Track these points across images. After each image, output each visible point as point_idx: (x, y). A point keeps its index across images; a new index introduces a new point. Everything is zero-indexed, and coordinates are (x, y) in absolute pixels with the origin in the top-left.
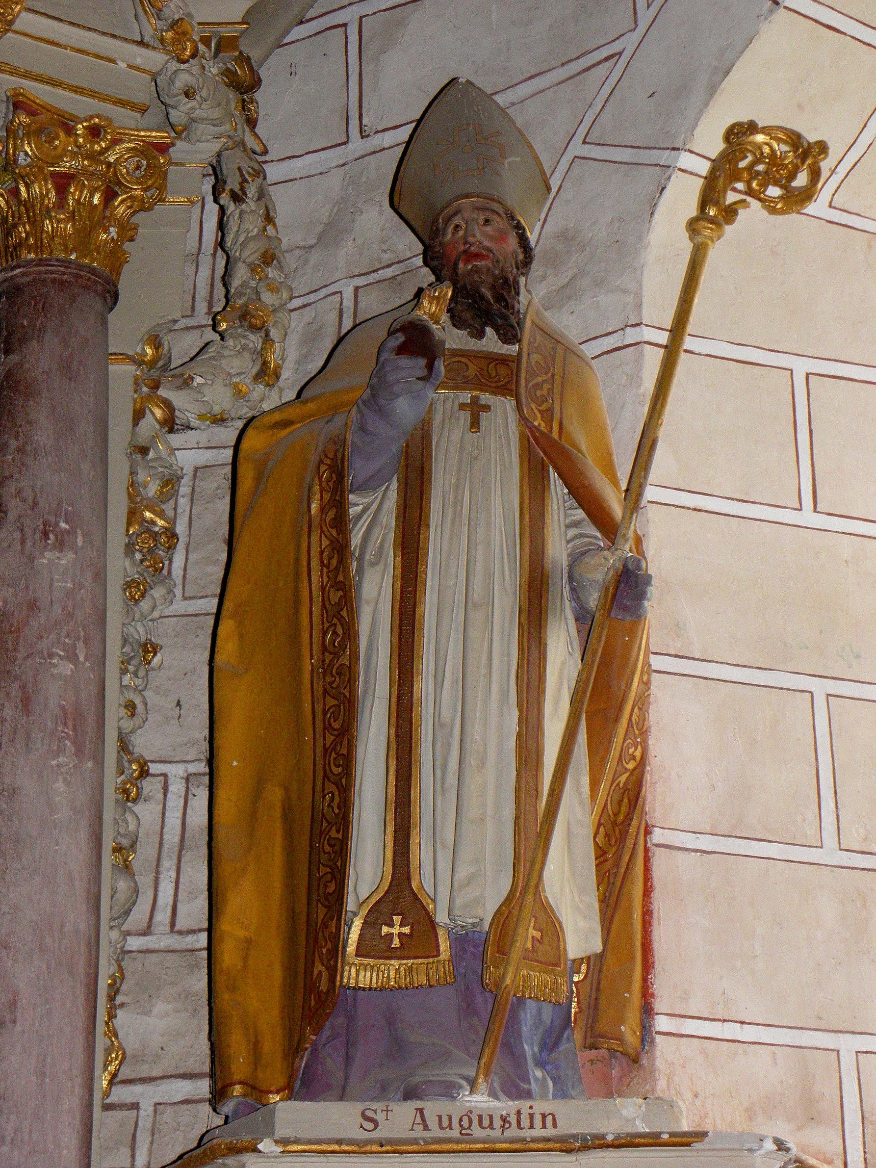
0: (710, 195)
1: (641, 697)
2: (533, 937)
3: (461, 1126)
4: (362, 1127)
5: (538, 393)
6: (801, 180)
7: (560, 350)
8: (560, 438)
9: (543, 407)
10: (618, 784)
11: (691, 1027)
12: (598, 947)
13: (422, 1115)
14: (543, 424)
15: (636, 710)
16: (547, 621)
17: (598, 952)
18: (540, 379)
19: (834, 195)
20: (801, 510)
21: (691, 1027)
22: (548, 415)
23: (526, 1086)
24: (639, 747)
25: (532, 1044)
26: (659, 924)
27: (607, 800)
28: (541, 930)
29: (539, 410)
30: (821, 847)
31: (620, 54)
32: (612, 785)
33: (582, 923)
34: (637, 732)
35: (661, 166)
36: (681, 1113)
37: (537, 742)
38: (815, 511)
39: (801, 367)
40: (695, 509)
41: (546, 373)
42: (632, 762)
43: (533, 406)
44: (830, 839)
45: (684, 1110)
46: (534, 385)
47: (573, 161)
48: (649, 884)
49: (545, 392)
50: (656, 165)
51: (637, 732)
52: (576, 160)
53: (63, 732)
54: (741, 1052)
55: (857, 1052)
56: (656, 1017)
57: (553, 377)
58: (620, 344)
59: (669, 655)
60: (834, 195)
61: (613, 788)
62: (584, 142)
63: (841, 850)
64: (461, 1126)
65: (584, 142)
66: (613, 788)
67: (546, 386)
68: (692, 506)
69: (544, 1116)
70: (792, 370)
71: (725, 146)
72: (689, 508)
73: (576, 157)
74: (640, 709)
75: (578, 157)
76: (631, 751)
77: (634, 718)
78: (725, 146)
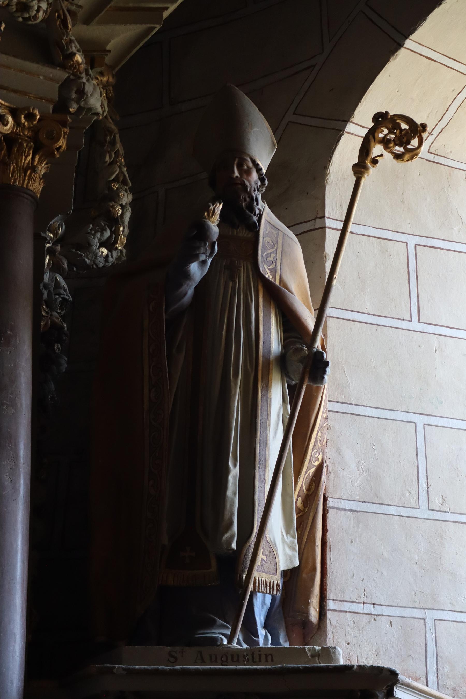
0: (365, 150)
1: (322, 426)
2: (262, 559)
3: (222, 660)
4: (169, 660)
6: (414, 143)
7: (280, 234)
8: (280, 284)
9: (271, 267)
10: (309, 474)
11: (346, 606)
12: (297, 563)
13: (201, 655)
14: (271, 277)
15: (319, 433)
17: (297, 566)
18: (270, 252)
19: (430, 146)
20: (411, 321)
21: (346, 606)
22: (274, 272)
23: (256, 639)
24: (321, 453)
25: (260, 616)
26: (330, 551)
27: (303, 482)
28: (265, 555)
29: (269, 269)
30: (419, 508)
31: (314, 66)
32: (305, 474)
33: (289, 552)
34: (320, 445)
35: (336, 130)
36: (339, 654)
37: (266, 453)
38: (419, 322)
39: (413, 241)
40: (353, 321)
41: (273, 248)
42: (317, 461)
43: (265, 266)
44: (423, 503)
45: (341, 653)
47: (288, 124)
48: (325, 529)
50: (334, 129)
51: (320, 445)
53: (9, 446)
54: (373, 620)
55: (435, 620)
56: (328, 601)
58: (312, 228)
59: (338, 402)
60: (430, 146)
61: (306, 476)
62: (294, 114)
63: (429, 510)
64: (222, 660)
65: (294, 114)
66: (306, 476)
67: (273, 255)
69: (266, 656)
70: (407, 243)
71: (373, 124)
72: (350, 320)
74: (321, 432)
76: (316, 455)
77: (318, 437)
78: (373, 124)
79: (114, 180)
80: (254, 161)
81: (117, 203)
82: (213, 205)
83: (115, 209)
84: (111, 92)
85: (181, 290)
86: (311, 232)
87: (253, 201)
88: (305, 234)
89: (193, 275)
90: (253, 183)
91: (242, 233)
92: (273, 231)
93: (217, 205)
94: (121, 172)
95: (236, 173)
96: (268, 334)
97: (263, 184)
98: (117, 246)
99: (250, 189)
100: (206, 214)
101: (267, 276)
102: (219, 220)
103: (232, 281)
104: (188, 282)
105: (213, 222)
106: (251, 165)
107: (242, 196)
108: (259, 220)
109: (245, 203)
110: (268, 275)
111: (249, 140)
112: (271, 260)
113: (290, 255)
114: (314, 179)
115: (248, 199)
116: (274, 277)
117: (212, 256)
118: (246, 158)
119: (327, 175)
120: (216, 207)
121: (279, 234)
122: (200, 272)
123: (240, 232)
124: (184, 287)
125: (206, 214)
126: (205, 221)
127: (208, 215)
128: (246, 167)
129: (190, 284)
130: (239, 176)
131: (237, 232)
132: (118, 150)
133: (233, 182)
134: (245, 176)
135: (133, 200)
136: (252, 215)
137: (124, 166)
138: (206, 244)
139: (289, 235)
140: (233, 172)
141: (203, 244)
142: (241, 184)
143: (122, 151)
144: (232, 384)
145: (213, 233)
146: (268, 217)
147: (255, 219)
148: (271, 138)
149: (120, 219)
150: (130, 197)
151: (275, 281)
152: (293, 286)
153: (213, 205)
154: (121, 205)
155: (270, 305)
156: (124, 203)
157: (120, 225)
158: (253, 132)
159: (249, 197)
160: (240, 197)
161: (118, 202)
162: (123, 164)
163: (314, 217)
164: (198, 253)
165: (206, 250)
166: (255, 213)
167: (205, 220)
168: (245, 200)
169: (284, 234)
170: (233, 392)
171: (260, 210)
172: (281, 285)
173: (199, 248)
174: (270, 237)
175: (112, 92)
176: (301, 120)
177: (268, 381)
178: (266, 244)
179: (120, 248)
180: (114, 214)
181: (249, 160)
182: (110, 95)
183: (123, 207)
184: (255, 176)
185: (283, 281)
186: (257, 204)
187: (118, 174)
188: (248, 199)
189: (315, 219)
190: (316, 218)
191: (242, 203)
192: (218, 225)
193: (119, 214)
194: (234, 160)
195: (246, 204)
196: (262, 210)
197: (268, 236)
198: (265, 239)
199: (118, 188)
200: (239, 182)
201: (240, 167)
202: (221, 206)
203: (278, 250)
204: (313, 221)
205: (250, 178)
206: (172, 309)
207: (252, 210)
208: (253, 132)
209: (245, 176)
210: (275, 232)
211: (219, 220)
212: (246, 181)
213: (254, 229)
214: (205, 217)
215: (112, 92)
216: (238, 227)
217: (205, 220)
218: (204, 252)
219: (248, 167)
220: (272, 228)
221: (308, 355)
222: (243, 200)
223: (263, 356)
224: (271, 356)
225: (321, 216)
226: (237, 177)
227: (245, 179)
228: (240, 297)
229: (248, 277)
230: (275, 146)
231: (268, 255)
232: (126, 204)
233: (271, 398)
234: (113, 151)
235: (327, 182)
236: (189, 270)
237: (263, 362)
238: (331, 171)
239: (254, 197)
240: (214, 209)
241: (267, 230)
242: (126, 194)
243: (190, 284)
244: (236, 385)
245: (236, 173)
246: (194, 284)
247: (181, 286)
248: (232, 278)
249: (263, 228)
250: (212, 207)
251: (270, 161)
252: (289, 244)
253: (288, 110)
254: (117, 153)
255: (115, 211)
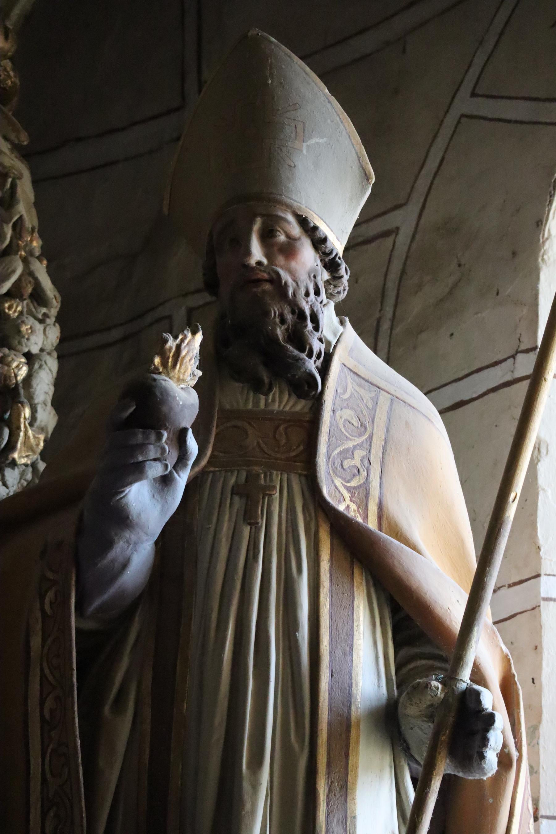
5: (346, 464)
7: (384, 399)
8: (380, 529)
9: (354, 483)
14: (353, 507)
16: (356, 776)
18: (350, 444)
22: (362, 495)
29: (348, 489)
41: (360, 435)
43: (338, 482)
46: (340, 453)
47: (459, 122)
49: (357, 461)
52: (464, 120)
57: (371, 438)
62: (474, 95)
65: (474, 95)
67: (359, 454)
68: (518, 616)
73: (463, 116)
75: (467, 116)
79: (9, 295)
80: (303, 222)
81: (15, 349)
82: (176, 338)
83: (9, 365)
84: (9, 76)
85: (111, 555)
86: (506, 390)
87: (301, 323)
88: (492, 395)
89: (139, 515)
90: (303, 277)
91: (280, 402)
92: (362, 392)
93: (185, 337)
94: (29, 273)
95: (257, 253)
96: (344, 652)
97: (335, 277)
98: (16, 455)
99: (294, 294)
100: (157, 360)
101: (341, 508)
102: (199, 373)
103: (250, 524)
104: (127, 534)
105: (179, 380)
106: (296, 230)
107: (275, 311)
108: (324, 370)
109: (283, 327)
110: (345, 505)
111: (292, 167)
112: (355, 466)
113: (408, 449)
114: (514, 254)
115: (289, 317)
116: (364, 507)
117: (185, 465)
118: (281, 214)
119: (544, 242)
120: (182, 341)
121: (381, 398)
122: (159, 507)
123: (273, 401)
124: (119, 549)
125: (157, 360)
126: (155, 380)
127: (164, 363)
128: (282, 238)
129: (133, 537)
130: (265, 261)
131: (266, 400)
132: (21, 217)
133: (249, 277)
134: (280, 260)
135: (62, 340)
136: (304, 356)
137: (39, 258)
138: (159, 437)
139: (409, 400)
140: (248, 253)
141: (153, 437)
142: (270, 281)
143: (31, 220)
144: (246, 785)
145: (177, 409)
146: (349, 359)
147: (312, 365)
148: (359, 158)
149: (24, 388)
150: (54, 334)
151: (366, 517)
152: (416, 527)
153: (176, 338)
154: (30, 357)
155: (352, 579)
156: (35, 350)
157: (22, 403)
158: (308, 146)
159: (293, 312)
160: (268, 313)
161: (19, 347)
162: (37, 253)
163: (512, 352)
164: (140, 459)
165: (163, 450)
166: (315, 351)
167: (156, 376)
168: (283, 321)
169: (394, 399)
170: (248, 806)
171: (328, 343)
172: (384, 526)
173: (142, 447)
174: (352, 408)
175: (12, 74)
176: (486, 108)
177: (347, 774)
178: (341, 426)
179: (23, 461)
180: (6, 377)
181: (290, 218)
182: (9, 82)
183: (30, 357)
184: (308, 257)
185: (388, 518)
186: (317, 328)
187: (19, 280)
188: (289, 317)
189: (513, 357)
190: (517, 352)
191: (274, 329)
192: (195, 387)
193: (20, 378)
194: (251, 223)
195: (287, 330)
196: (334, 344)
197: (348, 407)
198: (338, 414)
199: (21, 313)
200: (266, 276)
201: (267, 236)
202: (199, 337)
203: (374, 439)
204: (511, 360)
205: (293, 264)
206: (97, 603)
207: (301, 343)
208: (308, 146)
209: (280, 260)
210: (367, 395)
211: (199, 373)
212: (282, 273)
213: (310, 391)
214: (157, 369)
215: (12, 74)
216: (270, 389)
217: (156, 376)
218: (158, 455)
219: (288, 236)
220: (360, 385)
221: (444, 701)
222: (277, 320)
223: (330, 710)
224: (353, 708)
225: (529, 346)
226: (259, 263)
227: (281, 267)
228: (270, 562)
229: (291, 510)
230: (368, 179)
231: (348, 454)
232: (42, 350)
233: (354, 817)
234: (7, 223)
235: (543, 259)
236: (127, 504)
237: (330, 724)
238: (553, 232)
239: (308, 312)
240: (178, 347)
241: (345, 391)
242: (39, 327)
243: (133, 537)
244: (255, 786)
245: (257, 253)
246: (144, 538)
247: (109, 544)
248: (249, 516)
249: (336, 389)
250: (171, 343)
251: (356, 216)
252: (407, 423)
253: (460, 85)
254: (18, 226)
255: (9, 371)
